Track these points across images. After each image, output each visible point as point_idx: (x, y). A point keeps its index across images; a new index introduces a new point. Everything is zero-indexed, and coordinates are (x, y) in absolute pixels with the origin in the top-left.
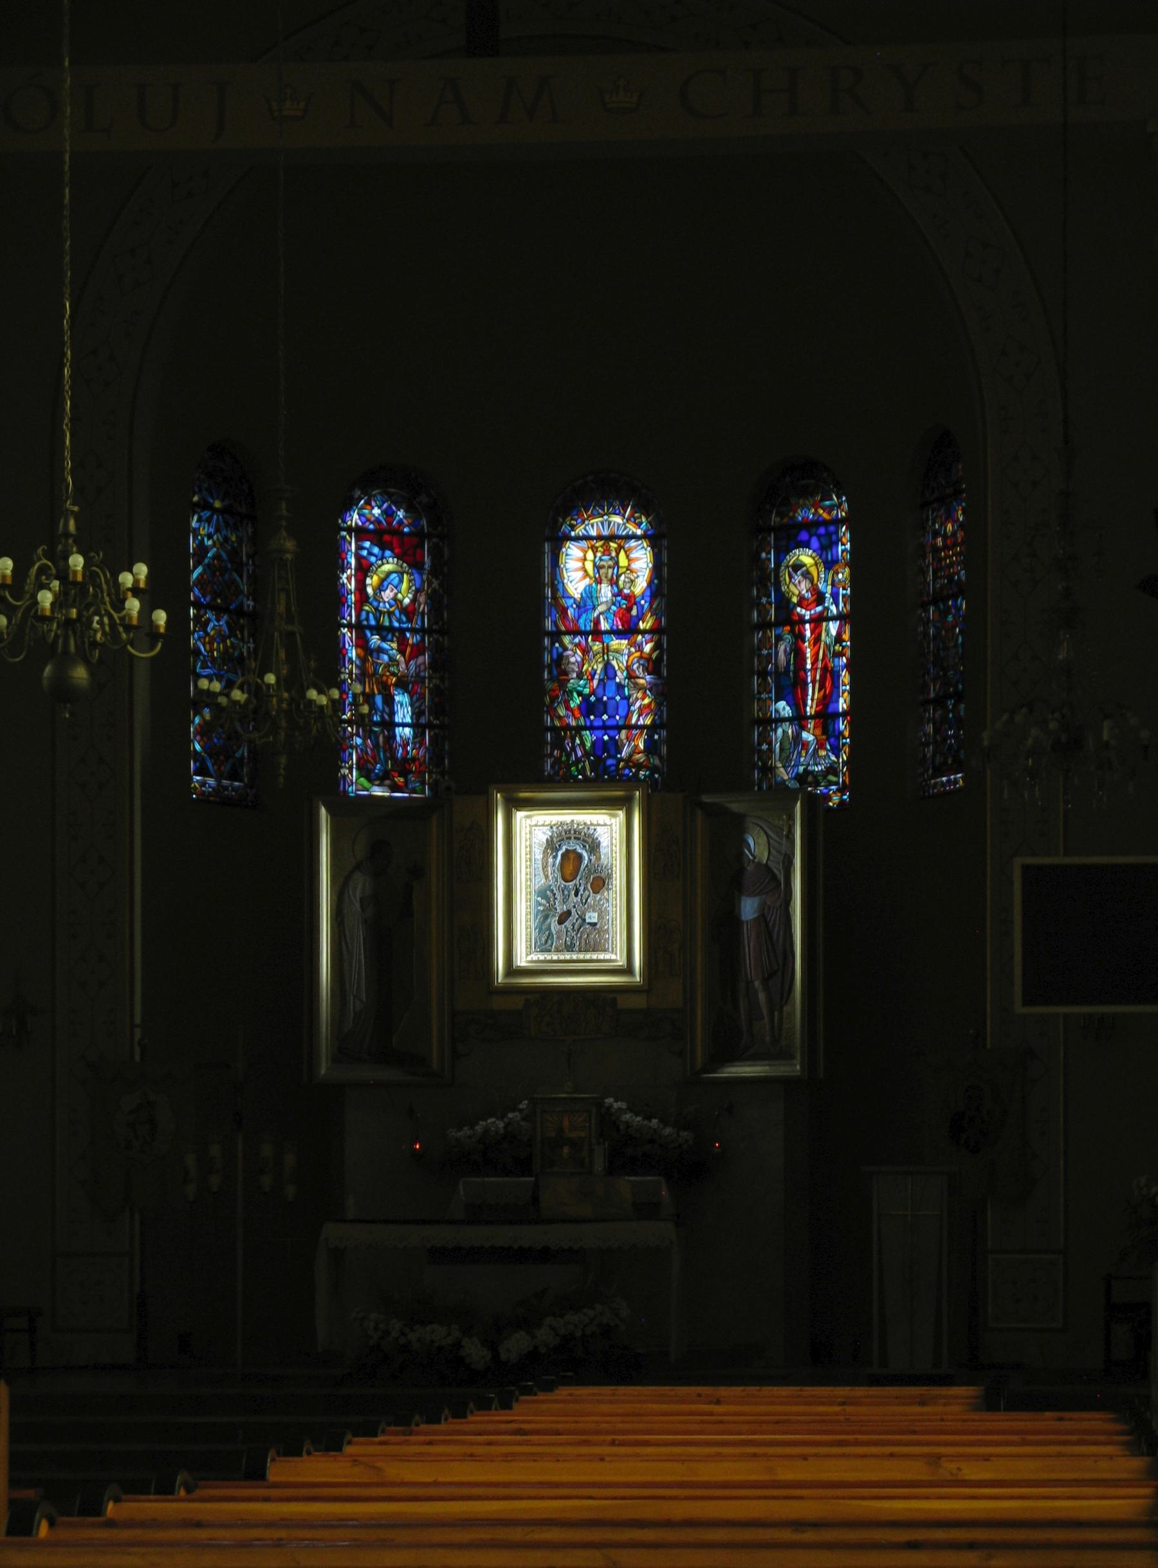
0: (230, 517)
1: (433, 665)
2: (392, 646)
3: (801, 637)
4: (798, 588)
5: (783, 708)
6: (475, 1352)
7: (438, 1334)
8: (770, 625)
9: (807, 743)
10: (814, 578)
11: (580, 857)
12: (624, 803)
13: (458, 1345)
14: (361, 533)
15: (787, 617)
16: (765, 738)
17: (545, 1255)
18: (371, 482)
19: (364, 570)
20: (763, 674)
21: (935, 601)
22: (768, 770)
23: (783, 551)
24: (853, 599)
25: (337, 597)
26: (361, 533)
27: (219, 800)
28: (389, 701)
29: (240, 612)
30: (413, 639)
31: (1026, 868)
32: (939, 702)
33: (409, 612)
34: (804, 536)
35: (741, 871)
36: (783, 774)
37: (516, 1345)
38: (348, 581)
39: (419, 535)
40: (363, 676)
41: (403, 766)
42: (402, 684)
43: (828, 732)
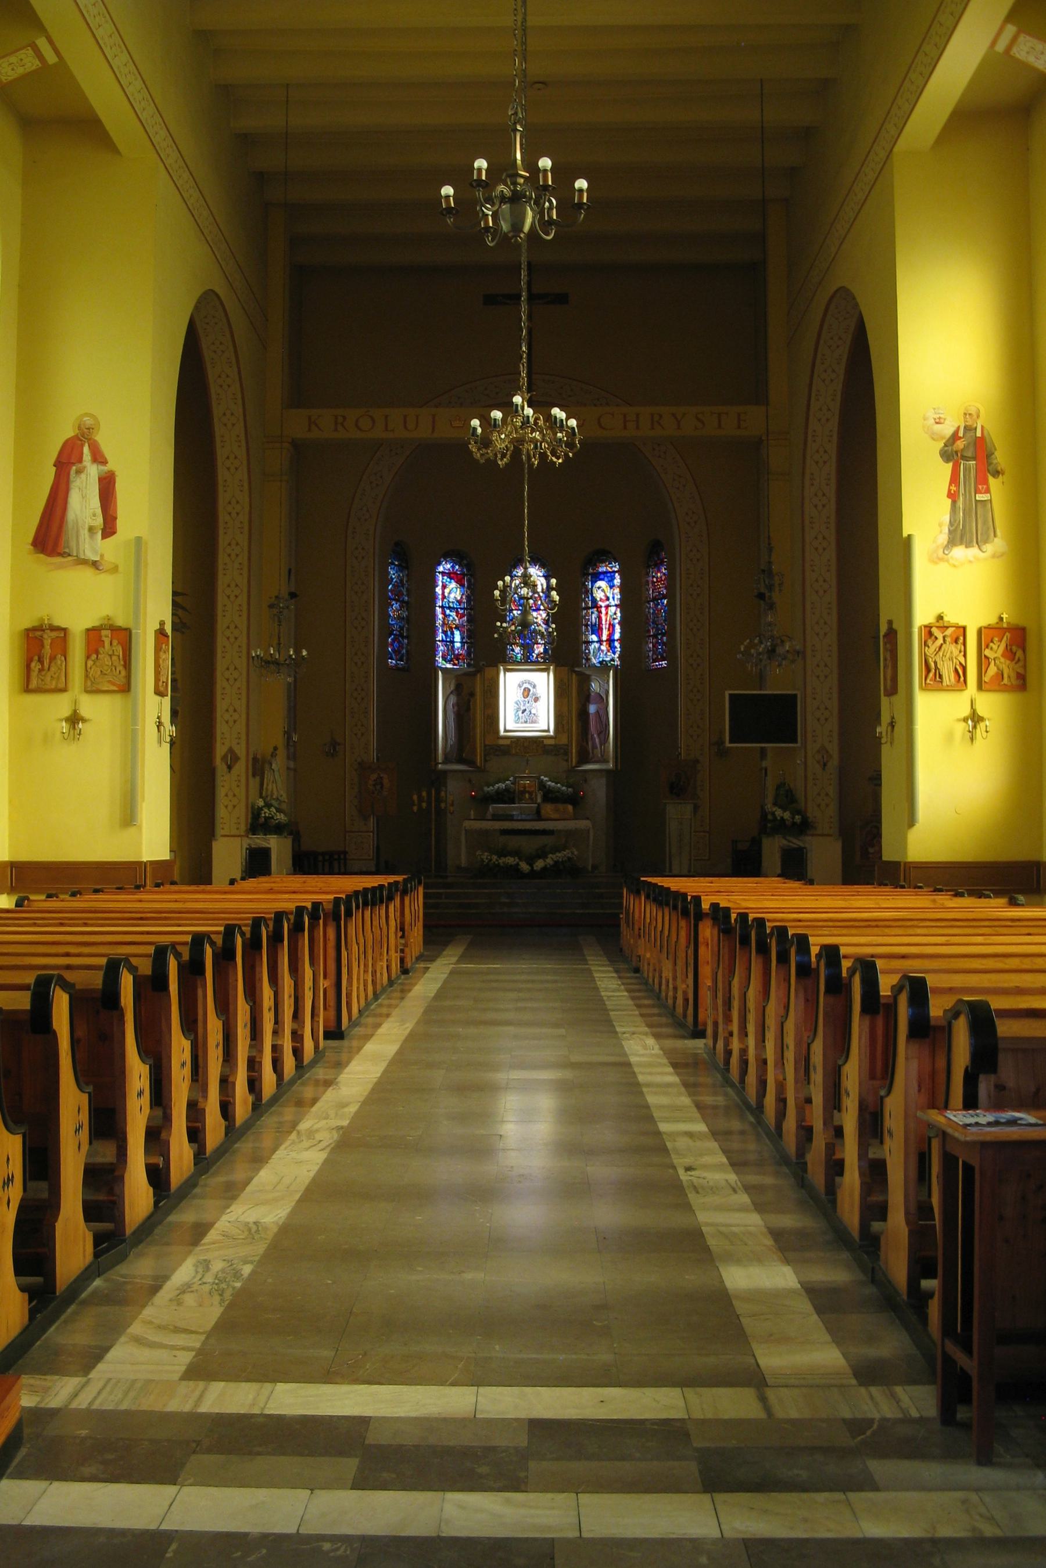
0: (401, 568)
1: (468, 621)
2: (454, 614)
3: (600, 612)
4: (599, 595)
5: (594, 638)
6: (524, 867)
7: (511, 860)
8: (589, 608)
9: (602, 650)
10: (607, 592)
11: (529, 690)
12: (547, 670)
13: (518, 864)
14: (443, 573)
15: (595, 605)
16: (587, 648)
17: (544, 832)
18: (447, 556)
19: (444, 587)
20: (587, 625)
21: (653, 601)
22: (588, 660)
23: (594, 582)
24: (621, 600)
25: (434, 597)
26: (443, 573)
27: (396, 668)
28: (453, 633)
29: (403, 602)
30: (461, 612)
31: (730, 695)
32: (655, 636)
33: (460, 602)
34: (602, 577)
35: (589, 695)
36: (594, 661)
37: (539, 864)
38: (439, 590)
39: (463, 574)
40: (444, 624)
41: (457, 657)
42: (457, 628)
43: (612, 647)
